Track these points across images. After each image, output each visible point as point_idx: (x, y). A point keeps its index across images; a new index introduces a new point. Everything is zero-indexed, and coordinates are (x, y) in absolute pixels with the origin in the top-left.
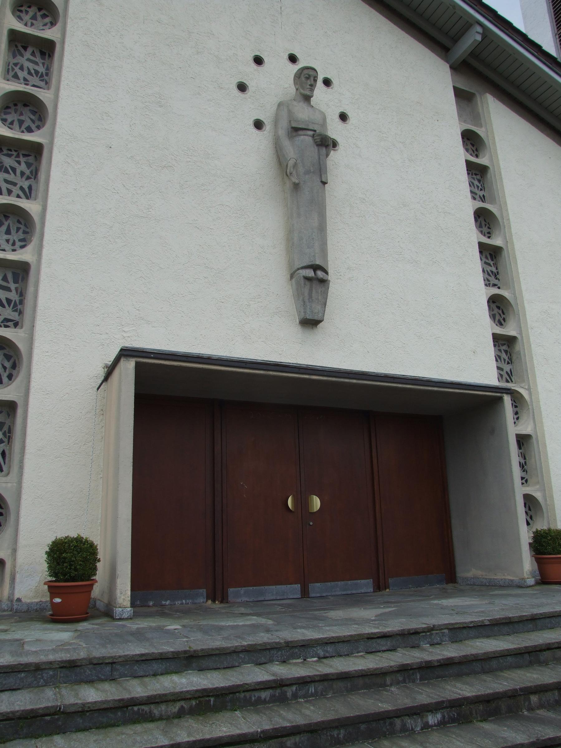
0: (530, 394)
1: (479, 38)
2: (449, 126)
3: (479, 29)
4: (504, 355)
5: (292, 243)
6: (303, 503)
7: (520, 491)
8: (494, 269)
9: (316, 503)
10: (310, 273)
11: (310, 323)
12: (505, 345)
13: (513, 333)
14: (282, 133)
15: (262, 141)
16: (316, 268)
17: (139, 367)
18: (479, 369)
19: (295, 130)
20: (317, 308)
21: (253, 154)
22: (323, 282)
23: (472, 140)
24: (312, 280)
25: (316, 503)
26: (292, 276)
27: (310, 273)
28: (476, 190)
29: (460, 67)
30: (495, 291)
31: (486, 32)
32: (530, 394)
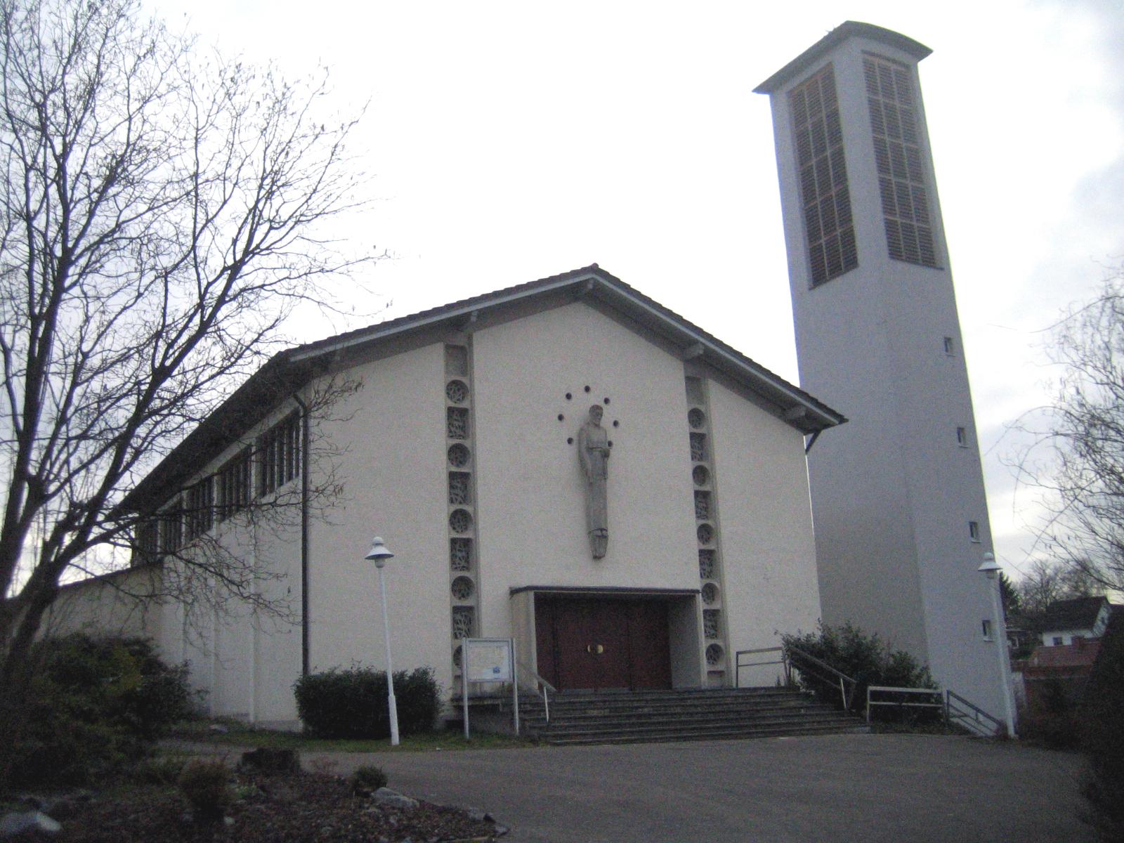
0: (721, 585)
1: (701, 352)
2: (681, 407)
3: (701, 346)
4: (706, 561)
5: (588, 510)
6: (594, 649)
7: (704, 644)
8: (705, 505)
9: (601, 649)
10: (599, 533)
11: (597, 558)
12: (708, 560)
13: (713, 548)
14: (584, 450)
15: (570, 453)
16: (602, 530)
17: (536, 594)
18: (687, 578)
19: (590, 450)
20: (602, 550)
21: (563, 460)
22: (605, 537)
23: (696, 417)
24: (598, 539)
25: (601, 649)
26: (590, 533)
27: (599, 533)
28: (696, 451)
29: (688, 362)
30: (703, 522)
31: (706, 348)
32: (721, 585)
